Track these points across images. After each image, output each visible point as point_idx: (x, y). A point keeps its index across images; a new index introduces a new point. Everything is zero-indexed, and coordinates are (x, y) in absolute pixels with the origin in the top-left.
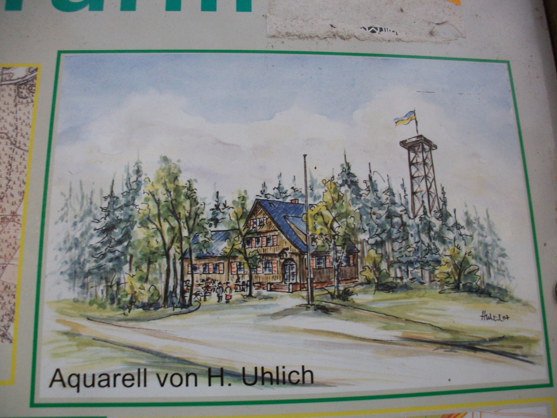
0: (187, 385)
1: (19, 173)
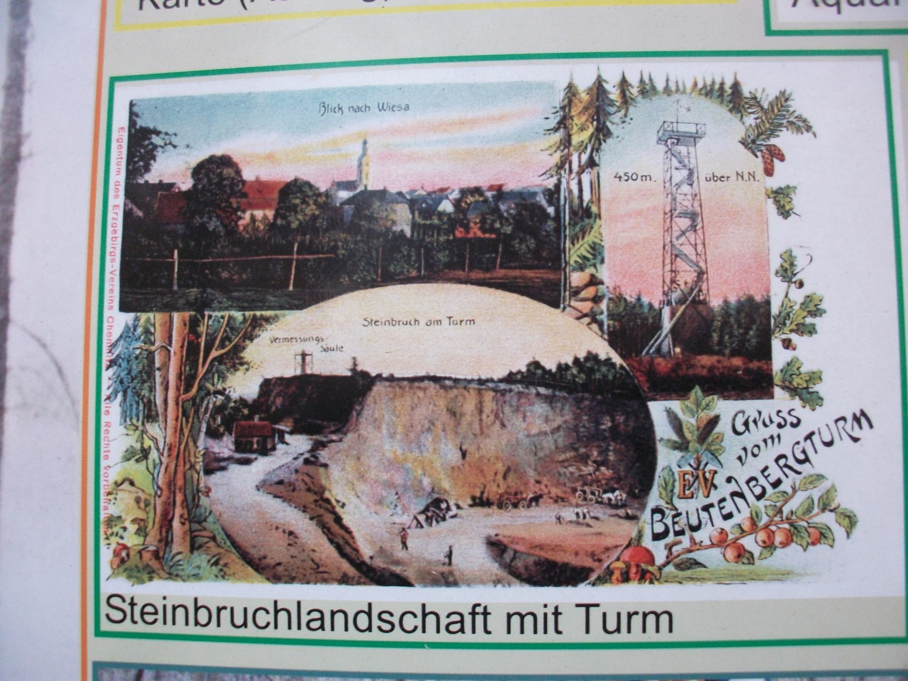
0: (245, 610)
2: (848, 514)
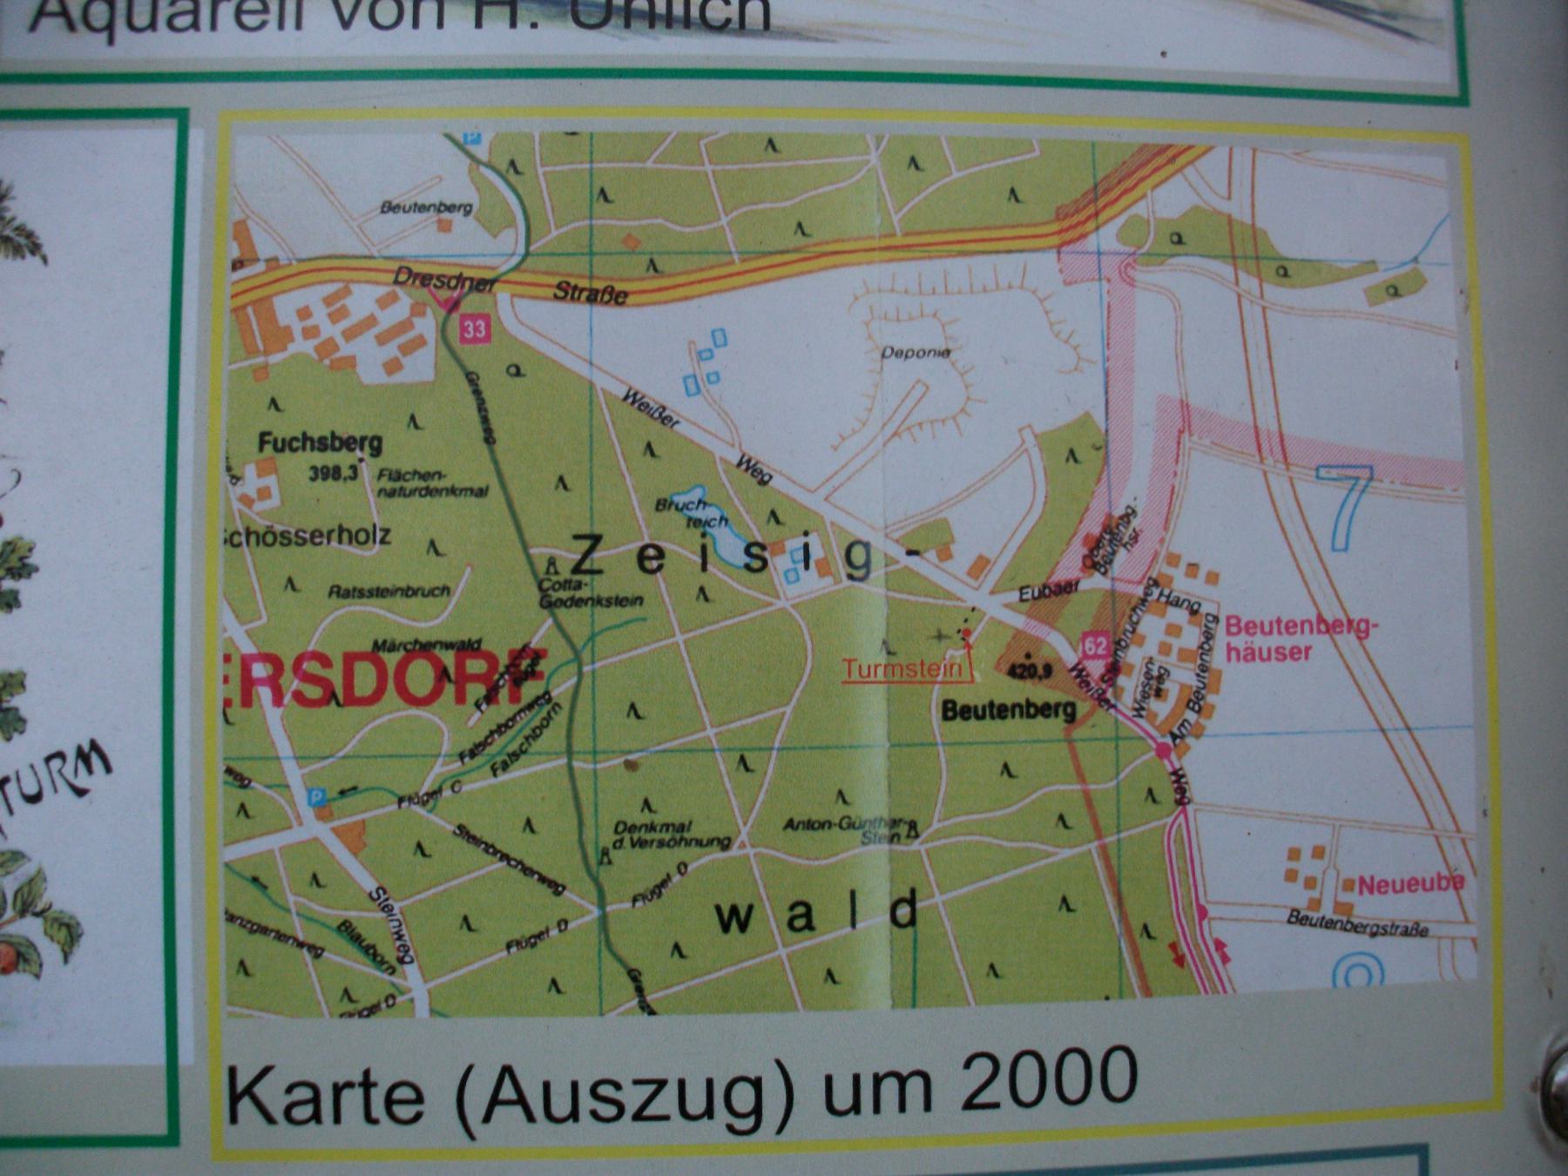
2: (66, 920)
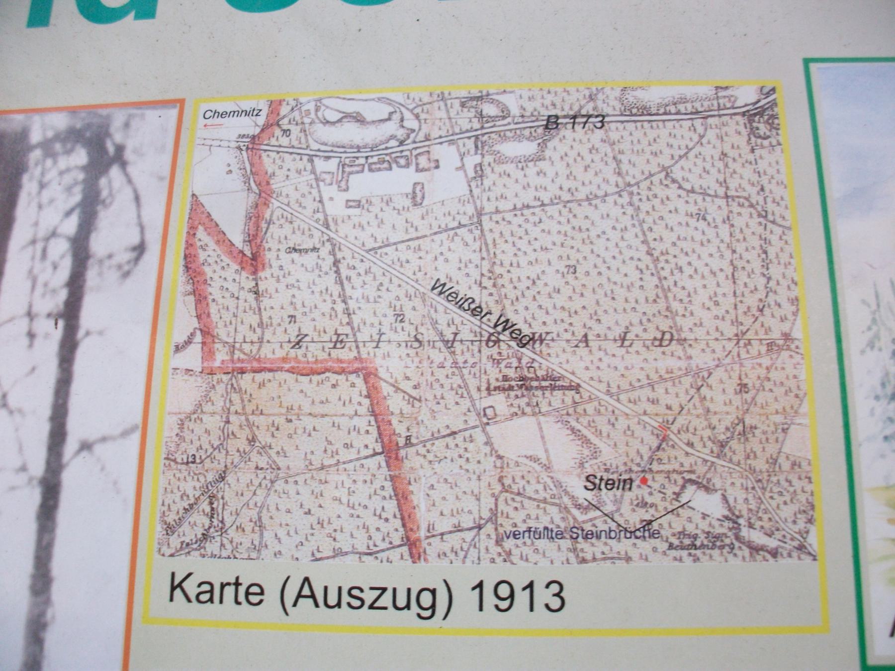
0: (409, 590)
1: (782, 266)
